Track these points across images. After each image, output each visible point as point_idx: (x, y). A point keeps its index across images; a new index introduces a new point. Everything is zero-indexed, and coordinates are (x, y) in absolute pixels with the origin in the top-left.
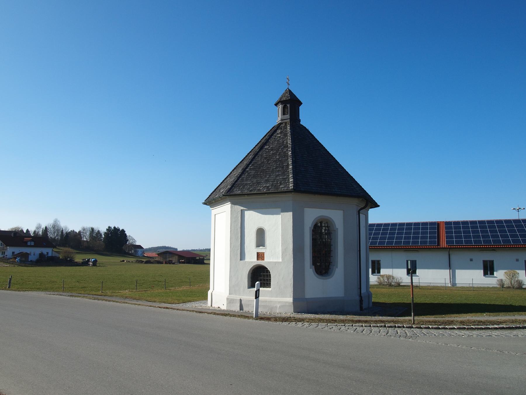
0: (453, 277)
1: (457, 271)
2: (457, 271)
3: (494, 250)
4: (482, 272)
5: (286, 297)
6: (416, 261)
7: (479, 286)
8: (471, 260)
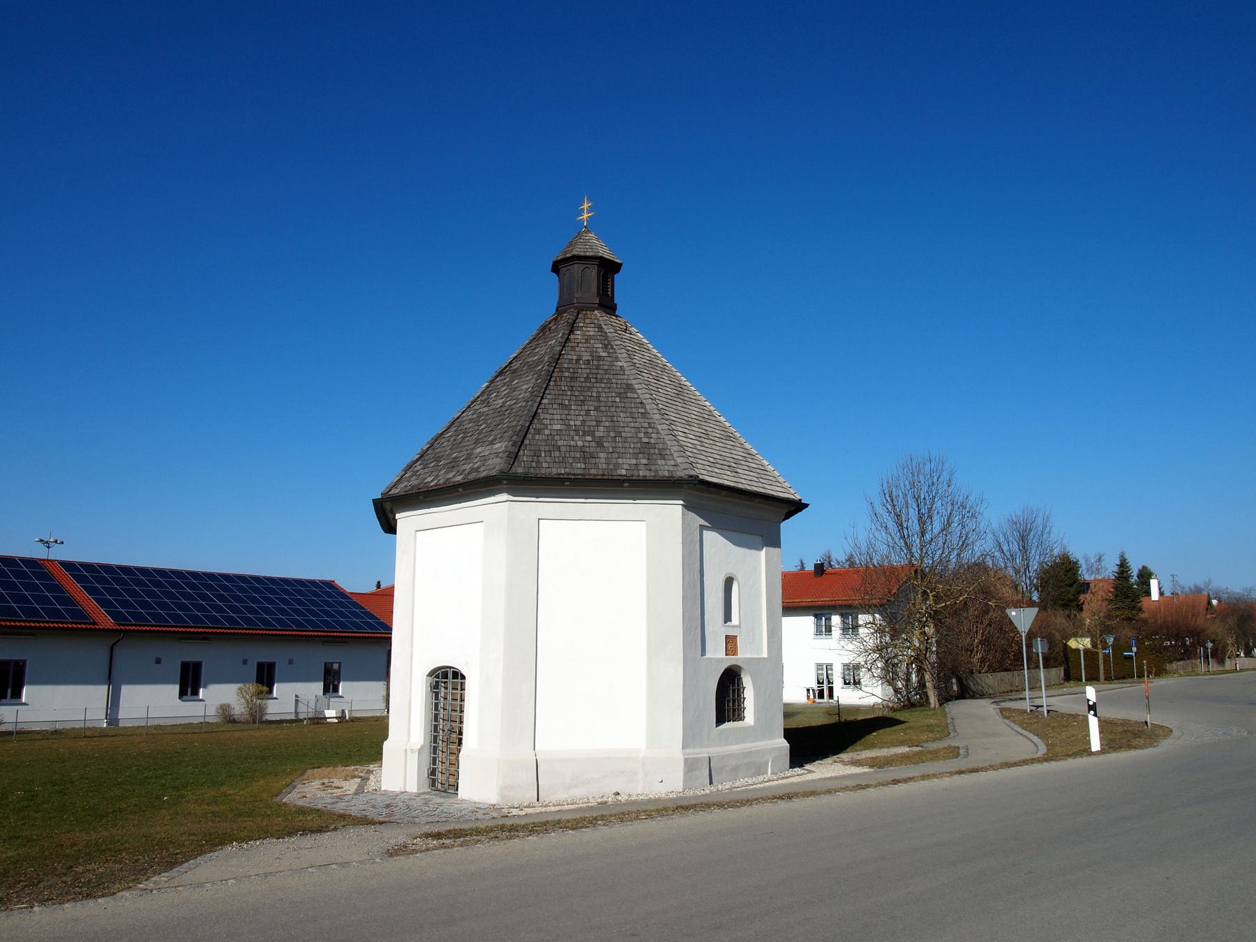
0: (114, 702)
1: (126, 690)
2: (126, 690)
3: (33, 635)
4: (176, 688)
5: (771, 738)
6: (24, 662)
7: (161, 722)
8: (158, 661)
